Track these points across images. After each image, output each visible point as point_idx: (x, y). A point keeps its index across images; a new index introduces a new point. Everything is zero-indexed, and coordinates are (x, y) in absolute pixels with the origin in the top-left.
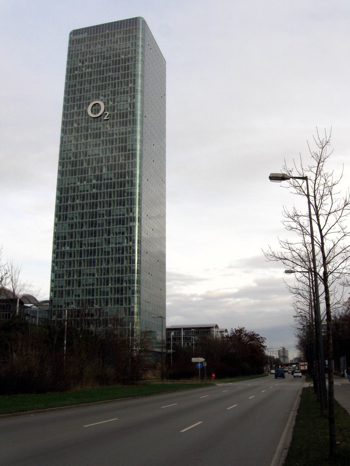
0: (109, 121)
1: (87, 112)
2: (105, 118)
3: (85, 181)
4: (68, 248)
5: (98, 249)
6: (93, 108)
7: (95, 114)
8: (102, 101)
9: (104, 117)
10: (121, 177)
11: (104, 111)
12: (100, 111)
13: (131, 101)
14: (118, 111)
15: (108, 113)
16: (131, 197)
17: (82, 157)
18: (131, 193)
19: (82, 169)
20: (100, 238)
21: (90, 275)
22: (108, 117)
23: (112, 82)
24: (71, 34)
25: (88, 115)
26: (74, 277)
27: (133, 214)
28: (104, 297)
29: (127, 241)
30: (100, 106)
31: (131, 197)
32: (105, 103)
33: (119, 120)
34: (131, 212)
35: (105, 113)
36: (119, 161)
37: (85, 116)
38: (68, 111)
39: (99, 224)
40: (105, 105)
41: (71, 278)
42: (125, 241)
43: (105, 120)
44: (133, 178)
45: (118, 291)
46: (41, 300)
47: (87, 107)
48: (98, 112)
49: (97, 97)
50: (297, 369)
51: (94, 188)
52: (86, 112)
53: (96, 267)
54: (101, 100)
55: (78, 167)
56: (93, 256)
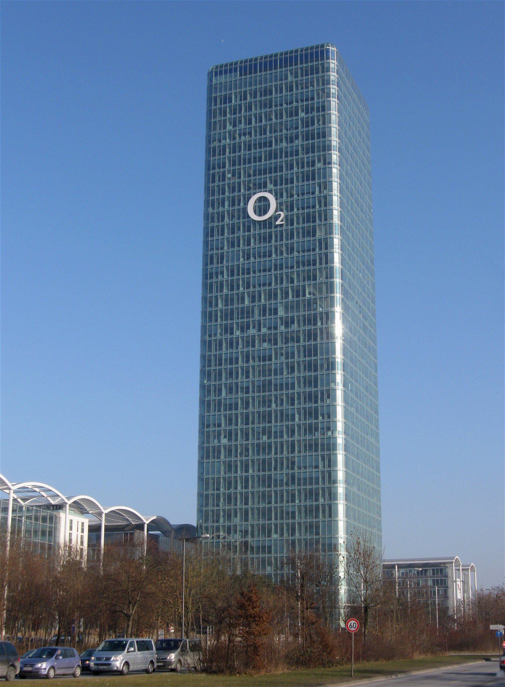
1: (247, 212)
4: (224, 441)
5: (276, 443)
7: (260, 215)
10: (308, 221)
11: (276, 211)
13: (320, 192)
14: (298, 209)
17: (241, 289)
18: (330, 545)
19: (243, 308)
20: (279, 424)
22: (282, 221)
23: (286, 159)
24: (210, 74)
25: (248, 217)
26: (236, 488)
27: (332, 434)
28: (287, 423)
29: (320, 188)
30: (269, 201)
32: (276, 195)
34: (329, 397)
35: (277, 213)
36: (304, 295)
37: (244, 218)
38: (209, 379)
41: (232, 490)
42: (317, 189)
44: (332, 502)
45: (310, 414)
47: (246, 203)
48: (265, 212)
49: (262, 186)
51: (264, 341)
52: (245, 210)
54: (270, 192)
55: (235, 306)
56: (268, 455)
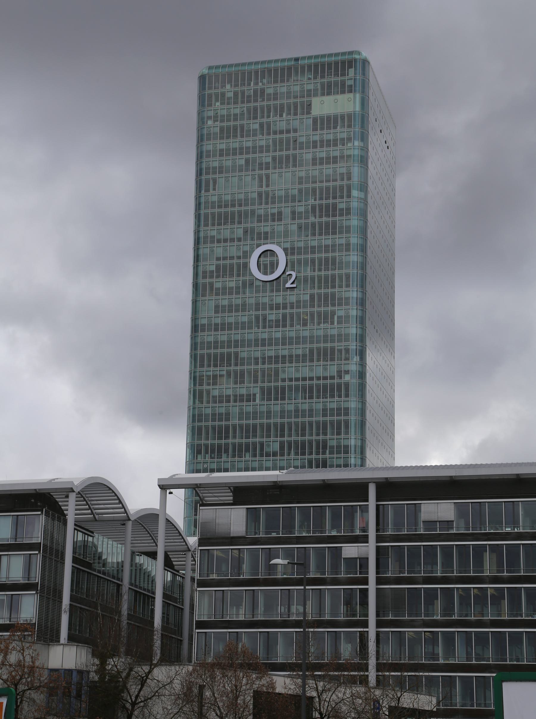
0: (295, 292)
2: (288, 285)
3: (218, 101)
6: (262, 259)
7: (265, 273)
8: (280, 246)
9: (286, 282)
12: (276, 269)
15: (294, 274)
16: (346, 418)
21: (225, 241)
25: (251, 274)
30: (277, 256)
31: (346, 418)
33: (55, 624)
35: (287, 273)
39: (332, 447)
40: (286, 255)
43: (287, 288)
46: (48, 478)
49: (266, 237)
50: (380, 506)
53: (259, 384)
